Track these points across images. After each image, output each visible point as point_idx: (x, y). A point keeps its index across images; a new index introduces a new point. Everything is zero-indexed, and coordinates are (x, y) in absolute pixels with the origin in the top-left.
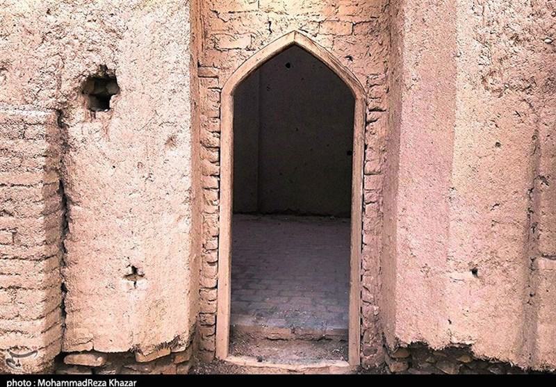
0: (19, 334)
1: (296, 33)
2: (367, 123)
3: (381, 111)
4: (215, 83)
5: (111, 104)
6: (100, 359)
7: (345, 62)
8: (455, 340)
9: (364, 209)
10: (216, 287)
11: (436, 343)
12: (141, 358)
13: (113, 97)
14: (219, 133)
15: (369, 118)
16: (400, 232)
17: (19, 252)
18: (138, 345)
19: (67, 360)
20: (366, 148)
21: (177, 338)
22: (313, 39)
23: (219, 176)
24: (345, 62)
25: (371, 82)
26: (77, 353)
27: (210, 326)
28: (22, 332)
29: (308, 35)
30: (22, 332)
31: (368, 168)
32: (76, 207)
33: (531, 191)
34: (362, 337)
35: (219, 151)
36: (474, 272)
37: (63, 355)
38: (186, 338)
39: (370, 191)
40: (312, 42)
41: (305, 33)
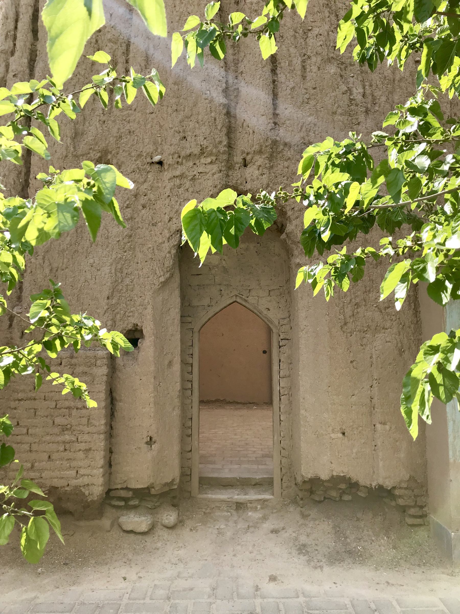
0: (90, 477)
1: (236, 296)
2: (280, 347)
3: (288, 339)
4: (190, 326)
5: (139, 345)
6: (131, 493)
7: (265, 312)
8: (335, 474)
9: (280, 399)
10: (191, 451)
11: (324, 476)
12: (153, 491)
13: (139, 340)
14: (192, 355)
15: (281, 344)
16: (302, 412)
17: (91, 429)
18: (153, 483)
19: (112, 494)
20: (280, 362)
21: (173, 480)
22: (246, 299)
23: (191, 381)
24: (265, 312)
25: (281, 323)
26: (118, 489)
27: (188, 475)
28: (92, 476)
29: (243, 297)
30: (92, 476)
31: (282, 373)
32: (120, 404)
33: (371, 387)
34: (282, 480)
35: (192, 366)
36: (344, 434)
37: (109, 491)
38: (178, 481)
39: (283, 388)
40: (246, 301)
41: (241, 296)
